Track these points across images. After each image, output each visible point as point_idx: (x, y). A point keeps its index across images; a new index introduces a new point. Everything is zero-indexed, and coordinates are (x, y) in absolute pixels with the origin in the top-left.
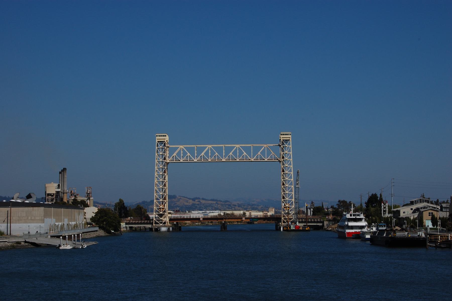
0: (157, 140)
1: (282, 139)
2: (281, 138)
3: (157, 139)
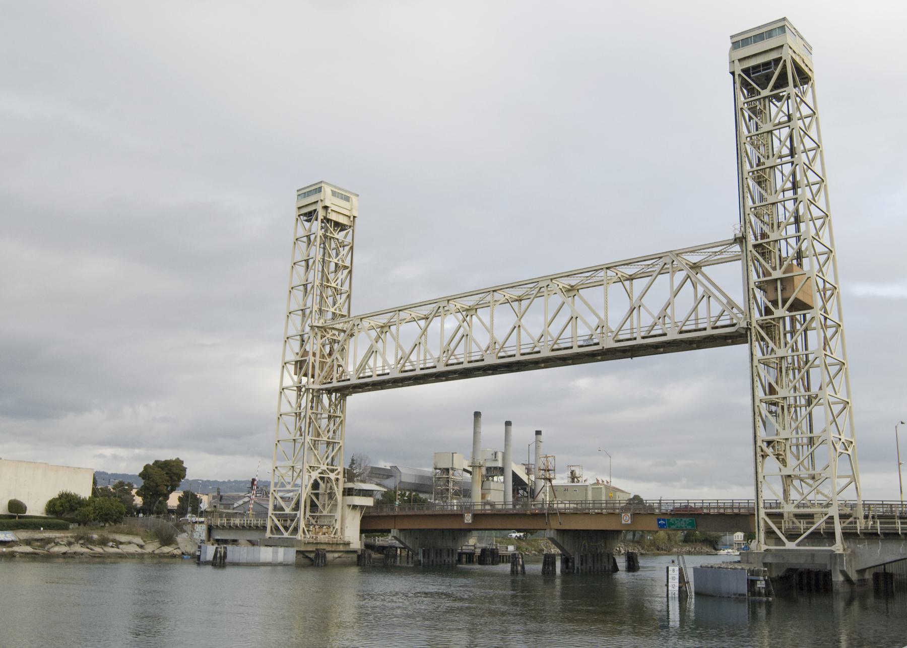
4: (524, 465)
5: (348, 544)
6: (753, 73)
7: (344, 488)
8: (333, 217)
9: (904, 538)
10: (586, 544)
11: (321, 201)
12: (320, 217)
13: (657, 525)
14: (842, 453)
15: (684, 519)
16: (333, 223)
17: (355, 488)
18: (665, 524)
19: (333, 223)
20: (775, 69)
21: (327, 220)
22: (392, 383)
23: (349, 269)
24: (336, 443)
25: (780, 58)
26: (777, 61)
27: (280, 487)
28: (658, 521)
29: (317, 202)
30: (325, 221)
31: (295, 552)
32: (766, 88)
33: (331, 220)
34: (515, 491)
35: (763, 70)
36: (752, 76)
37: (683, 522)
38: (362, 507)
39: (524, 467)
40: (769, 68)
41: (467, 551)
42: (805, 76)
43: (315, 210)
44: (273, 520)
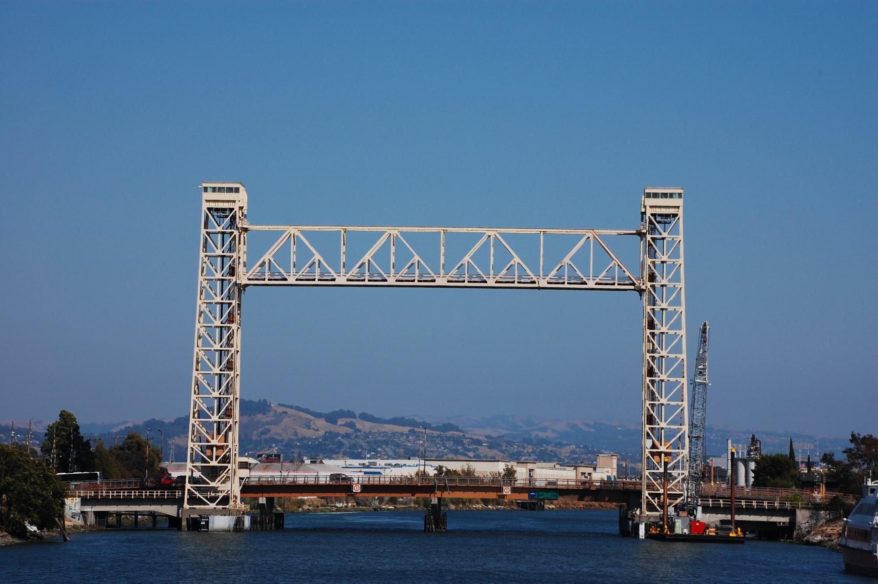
1: (649, 212)
2: (645, 207)
3: (207, 201)
17: (249, 462)
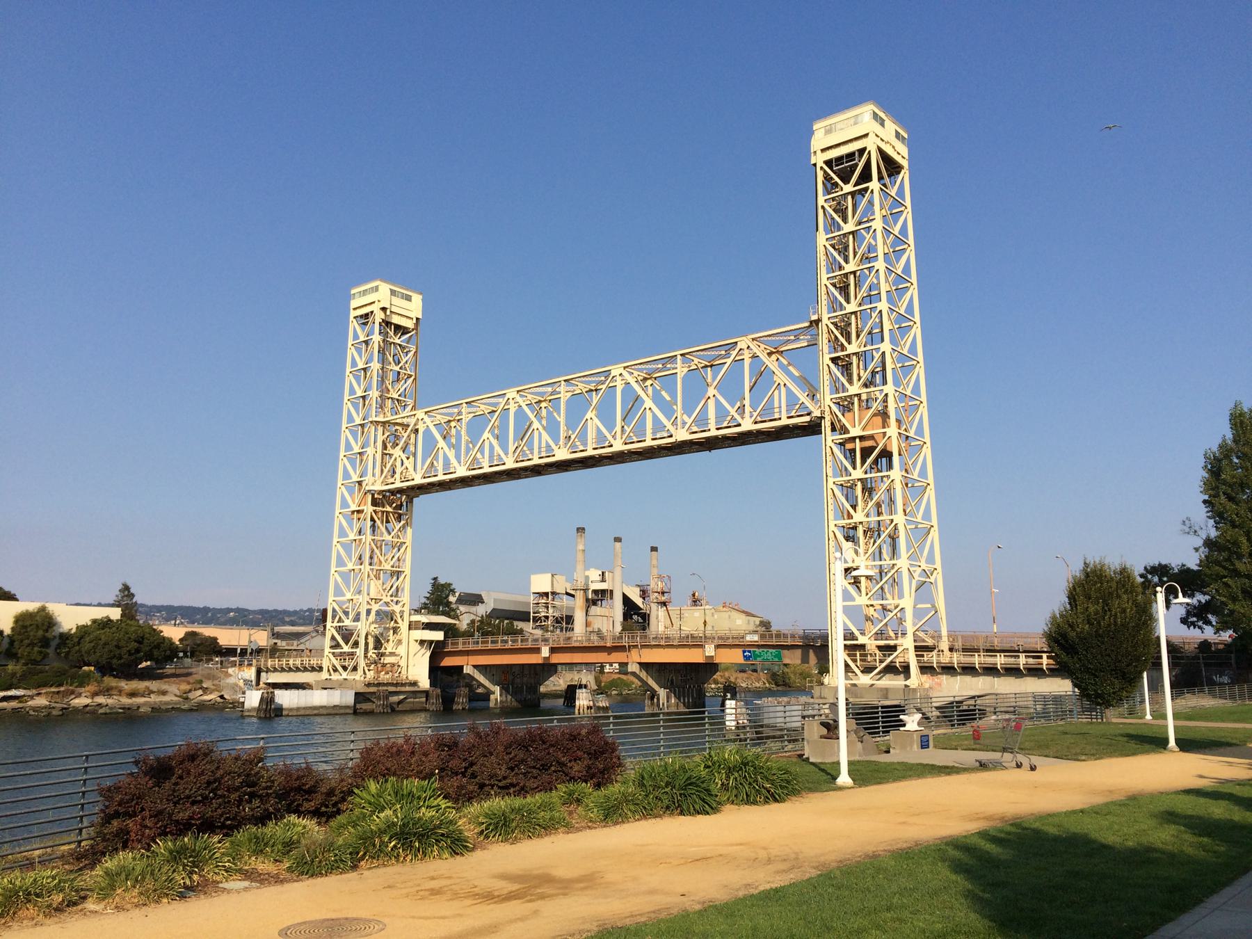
0: (353, 314)
3: (355, 309)
4: (639, 586)
5: (415, 684)
6: (837, 165)
7: (410, 622)
8: (396, 320)
9: (941, 672)
10: (674, 678)
11: (379, 301)
12: (378, 320)
13: (743, 657)
14: (926, 582)
15: (771, 650)
16: (393, 327)
18: (751, 656)
19: (393, 327)
20: (860, 161)
21: (387, 323)
22: (530, 471)
23: (413, 378)
24: (401, 572)
25: (865, 149)
26: (862, 151)
27: (338, 622)
28: (744, 653)
29: (374, 302)
30: (383, 324)
31: (354, 694)
32: (849, 183)
33: (391, 323)
34: (627, 616)
35: (847, 162)
36: (834, 169)
37: (769, 654)
38: (431, 642)
39: (638, 589)
40: (854, 160)
41: (969, 633)
42: (895, 166)
43: (372, 312)
44: (330, 660)
